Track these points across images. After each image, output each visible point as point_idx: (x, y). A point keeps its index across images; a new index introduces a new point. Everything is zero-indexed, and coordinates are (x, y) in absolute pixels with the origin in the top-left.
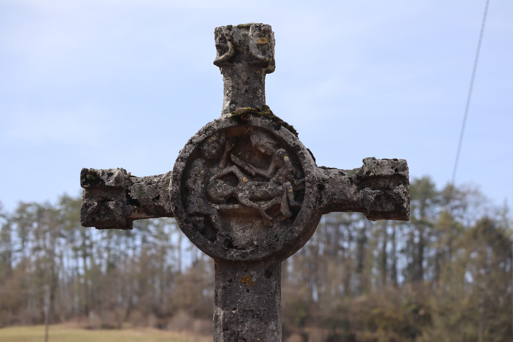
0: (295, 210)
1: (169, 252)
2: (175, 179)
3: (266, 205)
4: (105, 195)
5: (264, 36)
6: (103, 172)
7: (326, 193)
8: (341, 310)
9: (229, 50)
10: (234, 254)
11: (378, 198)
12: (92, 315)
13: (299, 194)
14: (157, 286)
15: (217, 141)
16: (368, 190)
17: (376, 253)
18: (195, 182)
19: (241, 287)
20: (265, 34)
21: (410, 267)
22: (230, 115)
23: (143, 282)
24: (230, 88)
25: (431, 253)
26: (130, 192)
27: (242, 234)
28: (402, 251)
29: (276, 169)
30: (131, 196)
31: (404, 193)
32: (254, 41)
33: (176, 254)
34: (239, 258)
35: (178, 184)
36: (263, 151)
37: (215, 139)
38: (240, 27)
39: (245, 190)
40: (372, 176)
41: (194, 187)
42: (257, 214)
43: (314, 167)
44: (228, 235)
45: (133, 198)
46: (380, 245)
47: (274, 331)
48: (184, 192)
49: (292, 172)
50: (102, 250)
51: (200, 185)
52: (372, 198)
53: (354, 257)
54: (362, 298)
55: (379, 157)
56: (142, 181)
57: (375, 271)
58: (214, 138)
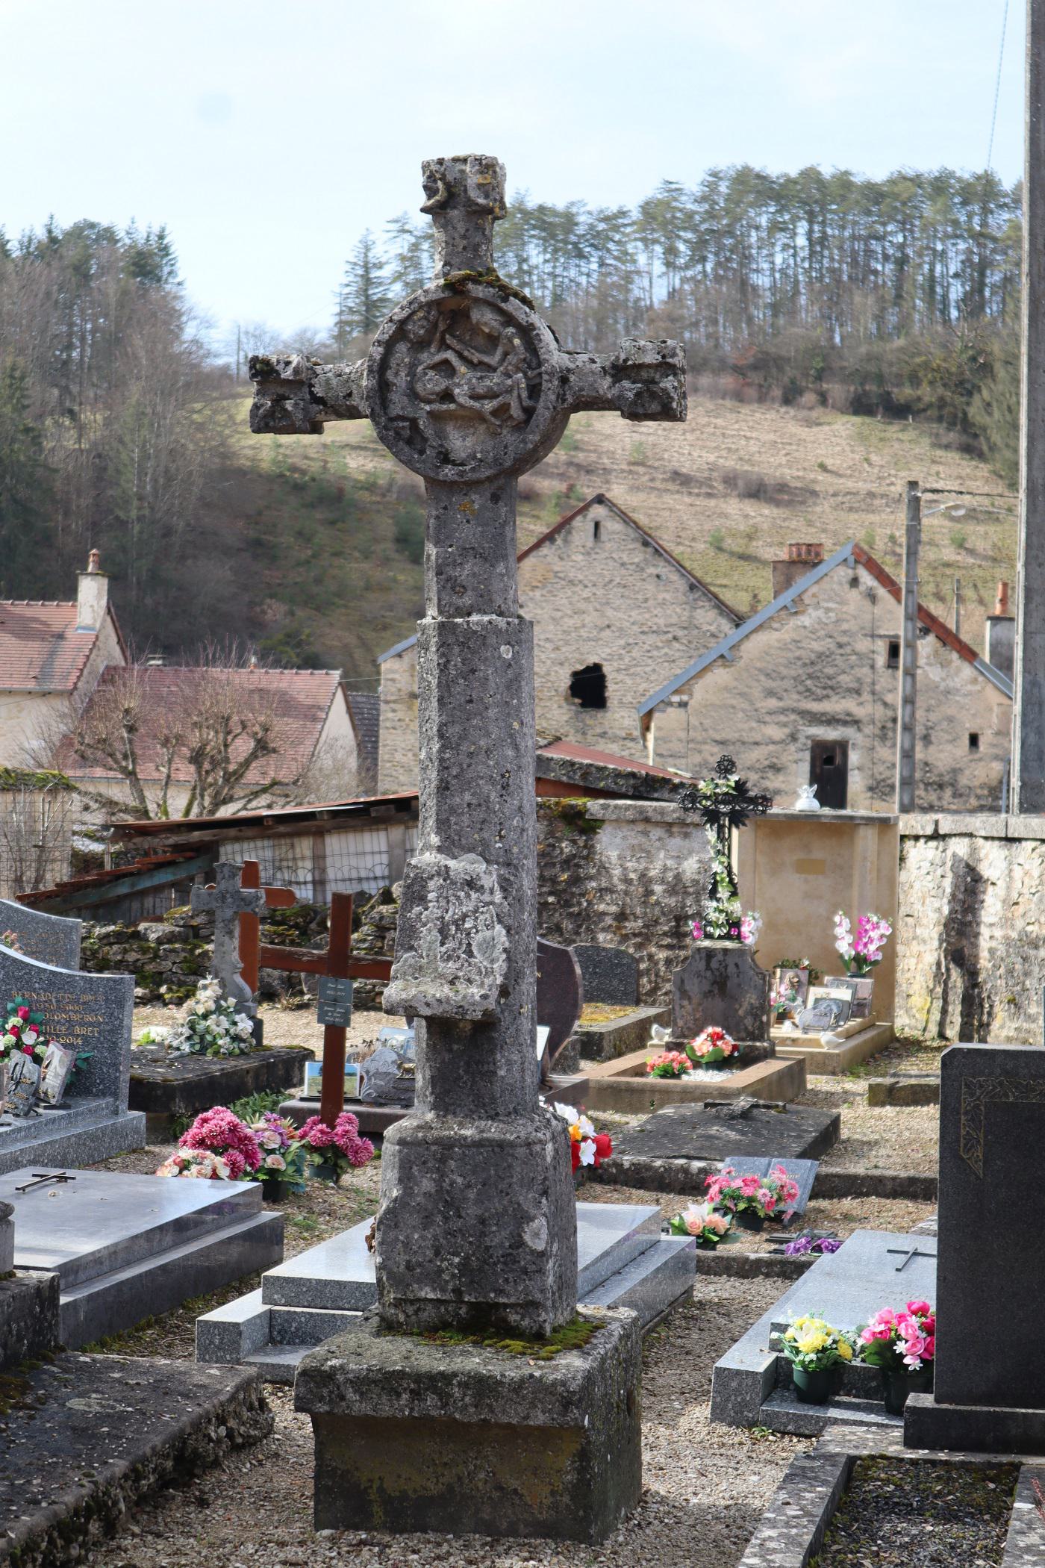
0: (529, 412)
2: (370, 371)
4: (281, 391)
7: (570, 388)
8: (870, 358)
10: (449, 472)
11: (638, 395)
13: (534, 391)
15: (425, 318)
16: (626, 384)
18: (397, 374)
21: (966, 298)
22: (442, 282)
23: (600, 322)
25: (994, 277)
27: (461, 443)
28: (956, 275)
29: (506, 354)
32: (473, 179)
34: (456, 478)
36: (487, 330)
38: (455, 160)
42: (480, 417)
44: (441, 446)
46: (926, 267)
47: (503, 575)
48: (383, 388)
49: (525, 360)
52: (630, 395)
54: (900, 342)
58: (421, 314)
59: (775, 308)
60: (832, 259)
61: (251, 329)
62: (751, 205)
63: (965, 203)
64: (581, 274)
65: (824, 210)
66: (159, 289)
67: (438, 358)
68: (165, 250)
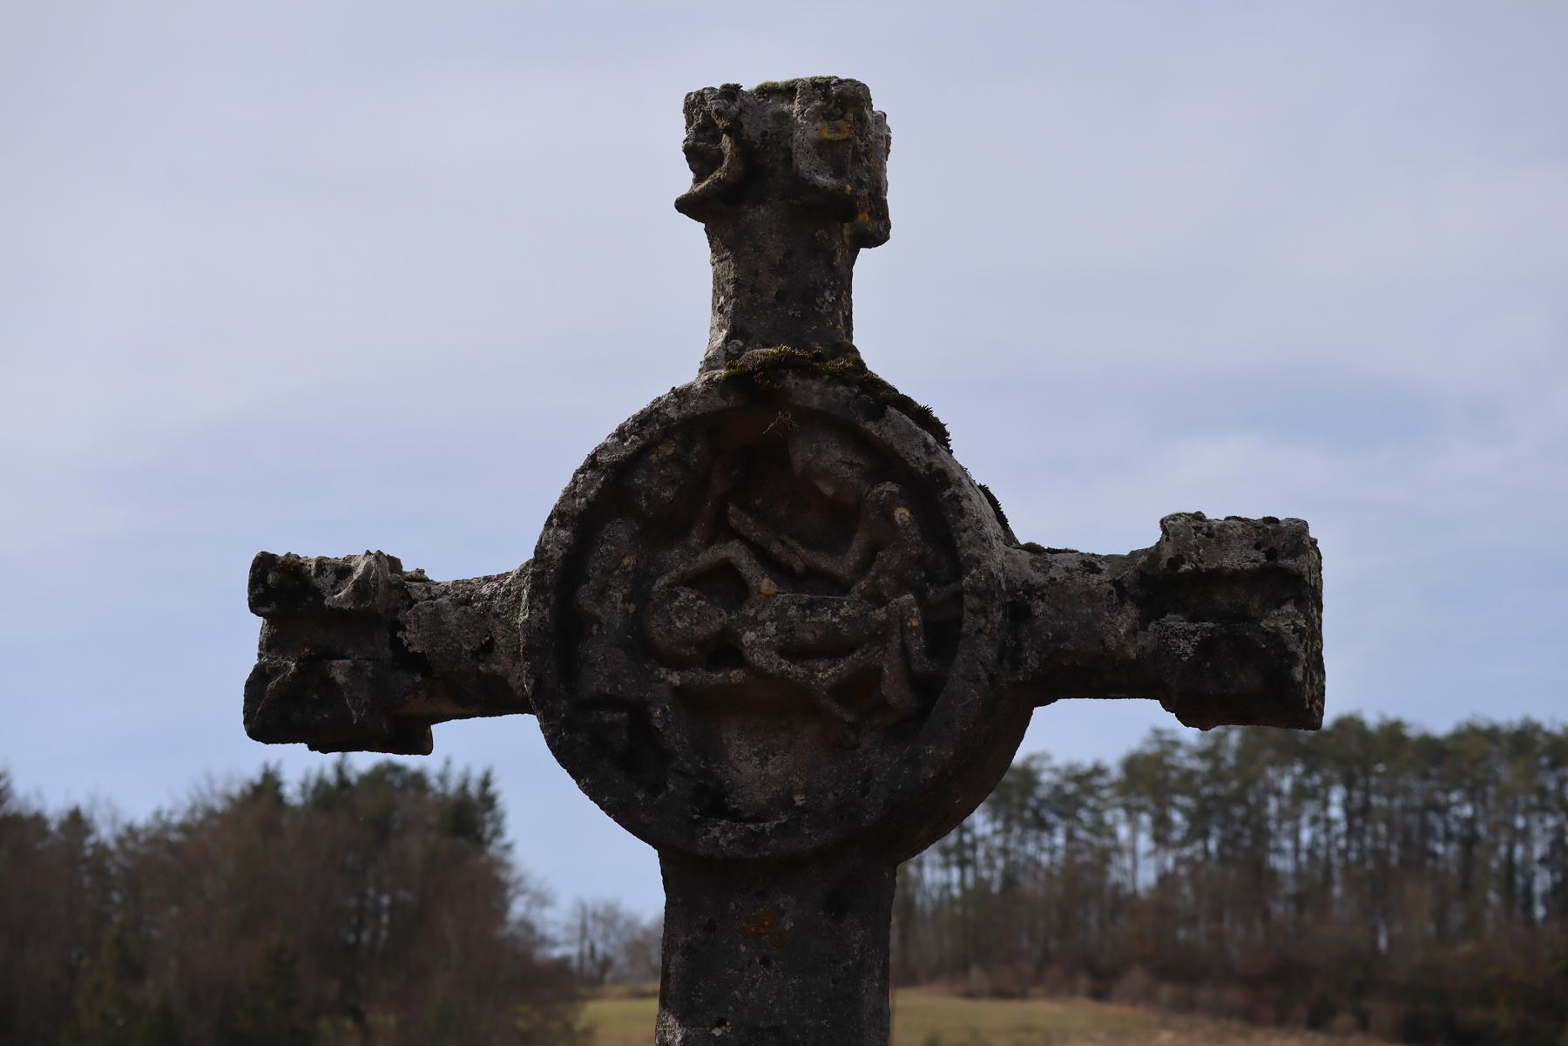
0: (927, 689)
1: (1115, 857)
2: (538, 588)
3: (831, 671)
5: (841, 117)
6: (321, 563)
9: (726, 162)
10: (721, 835)
11: (1205, 647)
12: (975, 973)
13: (943, 634)
14: (1093, 921)
16: (1175, 621)
17: (1494, 864)
18: (602, 594)
19: (743, 948)
20: (844, 111)
22: (721, 373)
24: (729, 288)
26: (404, 629)
27: (755, 767)
28: (1543, 861)
30: (405, 642)
31: (1294, 631)
33: (1127, 862)
35: (546, 603)
36: (828, 490)
37: (670, 452)
38: (767, 91)
39: (764, 622)
40: (1187, 572)
41: (598, 611)
43: (999, 545)
45: (411, 649)
46: (1503, 850)
50: (995, 853)
51: (619, 605)
52: (1186, 647)
53: (1453, 870)
55: (1216, 513)
56: (446, 593)
57: (1493, 897)
58: (668, 450)
59: (1300, 900)
60: (1376, 837)
61: (600, 910)
62: (1272, 763)
63: (1554, 765)
64: (1042, 849)
65: (1367, 773)
66: (483, 852)
67: (706, 558)
68: (488, 801)
